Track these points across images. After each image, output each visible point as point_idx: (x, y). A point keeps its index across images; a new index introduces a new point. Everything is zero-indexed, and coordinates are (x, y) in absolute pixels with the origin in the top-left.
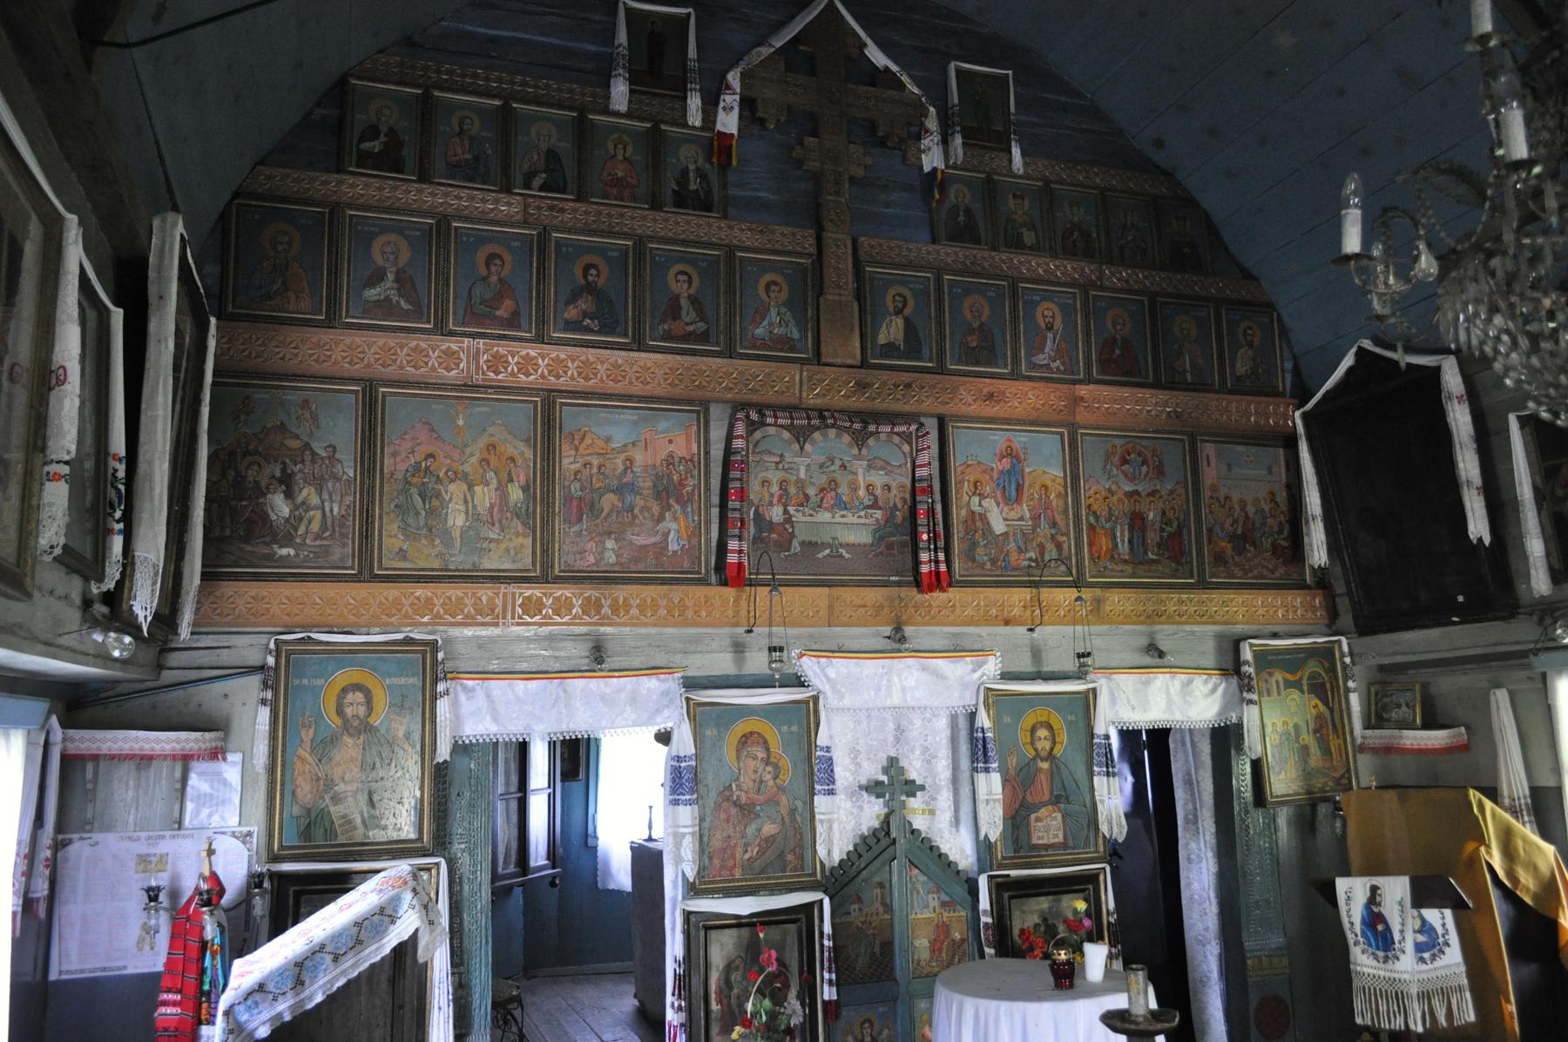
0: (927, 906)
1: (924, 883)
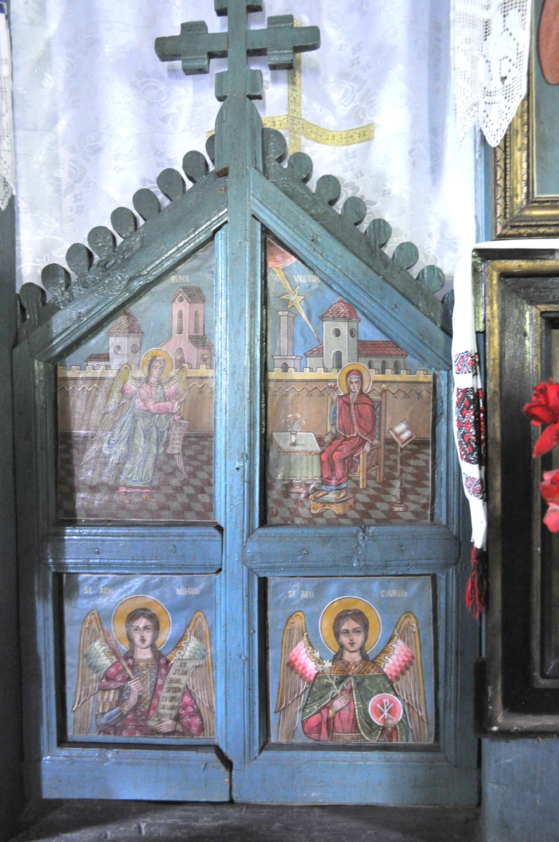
0: (319, 352)
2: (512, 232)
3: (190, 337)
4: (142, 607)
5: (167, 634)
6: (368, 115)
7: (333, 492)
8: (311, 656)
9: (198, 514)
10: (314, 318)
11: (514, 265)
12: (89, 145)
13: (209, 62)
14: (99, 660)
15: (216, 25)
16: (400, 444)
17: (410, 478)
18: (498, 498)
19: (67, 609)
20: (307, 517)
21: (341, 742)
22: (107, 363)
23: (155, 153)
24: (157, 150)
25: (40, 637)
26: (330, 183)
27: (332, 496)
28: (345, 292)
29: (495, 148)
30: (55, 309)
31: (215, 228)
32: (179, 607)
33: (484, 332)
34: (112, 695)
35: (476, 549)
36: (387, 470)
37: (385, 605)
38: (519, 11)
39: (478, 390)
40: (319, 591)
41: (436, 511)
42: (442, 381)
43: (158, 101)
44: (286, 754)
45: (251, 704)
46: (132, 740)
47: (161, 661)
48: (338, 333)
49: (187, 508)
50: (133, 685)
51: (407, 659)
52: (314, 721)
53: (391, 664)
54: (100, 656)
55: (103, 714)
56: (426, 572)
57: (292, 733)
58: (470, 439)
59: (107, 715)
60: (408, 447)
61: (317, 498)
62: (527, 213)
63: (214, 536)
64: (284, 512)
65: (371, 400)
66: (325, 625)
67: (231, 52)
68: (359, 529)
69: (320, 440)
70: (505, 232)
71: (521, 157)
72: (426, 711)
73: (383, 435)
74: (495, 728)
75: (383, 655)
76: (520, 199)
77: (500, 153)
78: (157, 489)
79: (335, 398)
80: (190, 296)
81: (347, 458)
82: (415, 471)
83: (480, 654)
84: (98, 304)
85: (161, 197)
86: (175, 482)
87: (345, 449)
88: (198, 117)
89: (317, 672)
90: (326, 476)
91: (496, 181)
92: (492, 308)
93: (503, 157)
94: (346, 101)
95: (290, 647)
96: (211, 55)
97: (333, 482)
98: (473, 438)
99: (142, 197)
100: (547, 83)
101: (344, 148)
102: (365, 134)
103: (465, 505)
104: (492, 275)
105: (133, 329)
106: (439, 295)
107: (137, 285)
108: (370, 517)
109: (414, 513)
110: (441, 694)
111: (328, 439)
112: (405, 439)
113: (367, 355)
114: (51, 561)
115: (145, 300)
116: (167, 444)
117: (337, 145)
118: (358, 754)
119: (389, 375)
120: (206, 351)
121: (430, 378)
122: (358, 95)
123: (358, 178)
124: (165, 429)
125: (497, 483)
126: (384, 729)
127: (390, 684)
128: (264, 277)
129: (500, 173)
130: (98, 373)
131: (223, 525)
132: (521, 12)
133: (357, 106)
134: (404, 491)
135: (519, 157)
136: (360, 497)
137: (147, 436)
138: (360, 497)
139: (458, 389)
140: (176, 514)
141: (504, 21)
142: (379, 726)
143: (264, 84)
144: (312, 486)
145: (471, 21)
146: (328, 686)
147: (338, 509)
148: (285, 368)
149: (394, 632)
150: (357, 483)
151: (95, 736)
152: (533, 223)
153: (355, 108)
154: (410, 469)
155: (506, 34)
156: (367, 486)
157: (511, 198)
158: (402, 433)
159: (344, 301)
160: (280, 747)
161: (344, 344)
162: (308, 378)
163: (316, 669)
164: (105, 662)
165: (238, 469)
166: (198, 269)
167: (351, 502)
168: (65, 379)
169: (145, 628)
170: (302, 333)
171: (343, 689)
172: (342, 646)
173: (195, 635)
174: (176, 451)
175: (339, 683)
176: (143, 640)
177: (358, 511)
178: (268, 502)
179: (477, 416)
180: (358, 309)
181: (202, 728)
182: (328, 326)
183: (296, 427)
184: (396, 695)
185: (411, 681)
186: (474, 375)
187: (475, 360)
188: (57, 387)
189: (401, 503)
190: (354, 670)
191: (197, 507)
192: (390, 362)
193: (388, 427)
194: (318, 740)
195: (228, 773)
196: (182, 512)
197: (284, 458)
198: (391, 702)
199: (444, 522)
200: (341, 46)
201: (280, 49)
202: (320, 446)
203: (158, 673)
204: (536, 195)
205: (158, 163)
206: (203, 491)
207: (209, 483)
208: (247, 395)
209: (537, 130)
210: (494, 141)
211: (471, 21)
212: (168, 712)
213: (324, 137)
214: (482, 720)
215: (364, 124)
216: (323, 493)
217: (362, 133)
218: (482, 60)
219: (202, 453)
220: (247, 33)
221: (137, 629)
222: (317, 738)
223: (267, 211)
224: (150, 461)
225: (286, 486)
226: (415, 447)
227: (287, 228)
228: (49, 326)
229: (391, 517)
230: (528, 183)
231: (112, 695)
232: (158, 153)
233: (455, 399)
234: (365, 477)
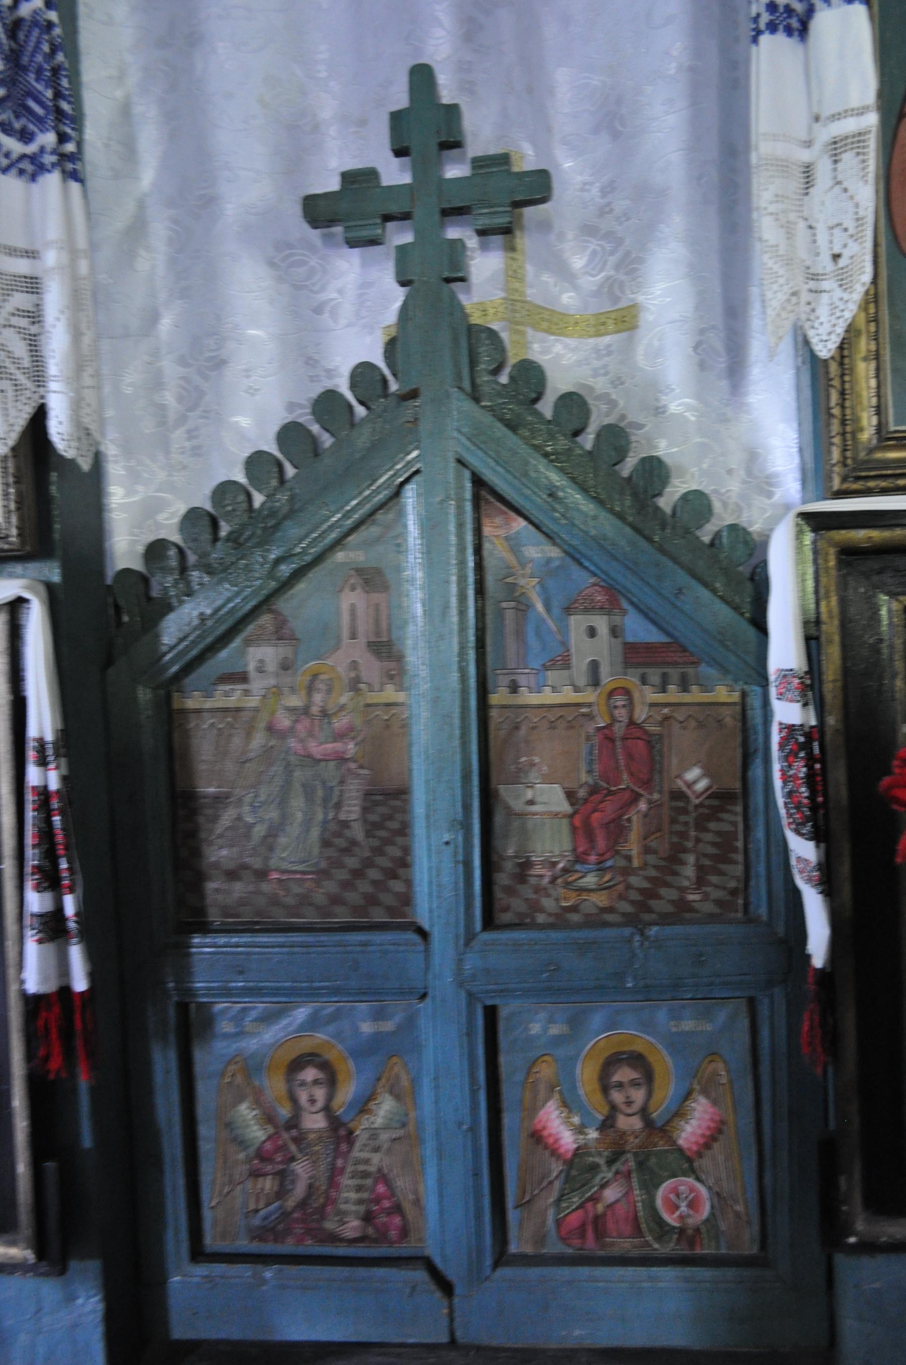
0: (564, 662)
1: (547, 571)
3: (370, 644)
4: (309, 1052)
5: (347, 1092)
6: (628, 292)
7: (594, 874)
8: (567, 1122)
10: (556, 611)
11: (860, 536)
12: (207, 355)
13: (384, 228)
14: (248, 1130)
15: (395, 173)
17: (711, 850)
18: (846, 891)
19: (199, 1056)
20: (555, 912)
21: (616, 1251)
22: (244, 686)
24: (310, 358)
25: (160, 1101)
26: (574, 404)
27: (590, 880)
28: (602, 571)
29: (826, 361)
30: (166, 607)
31: (401, 479)
32: (366, 1050)
33: (817, 638)
34: (268, 1184)
35: (816, 970)
36: (675, 839)
37: (677, 1044)
39: (812, 727)
40: (576, 1022)
41: (752, 899)
42: (755, 702)
43: (307, 283)
44: (534, 1272)
45: (478, 1197)
46: (301, 1250)
47: (340, 1132)
48: (592, 632)
49: (372, 901)
50: (301, 1169)
51: (712, 1125)
52: (575, 1219)
53: (689, 1132)
54: (248, 1126)
55: (256, 1211)
56: (738, 994)
57: (540, 1239)
58: (800, 802)
59: (262, 1213)
60: (707, 802)
62: (879, 455)
63: (414, 945)
64: (518, 905)
65: (646, 732)
66: (586, 1074)
67: (418, 213)
68: (635, 931)
69: (570, 795)
70: (845, 486)
71: (867, 370)
72: (745, 1204)
74: (852, 1240)
75: (676, 1120)
76: (867, 435)
77: (834, 368)
78: (324, 874)
80: (367, 582)
81: (613, 821)
82: (719, 840)
83: (826, 1125)
84: (229, 600)
85: (315, 428)
86: (352, 862)
87: (610, 808)
88: (369, 304)
89: (575, 1146)
90: (581, 849)
91: (829, 409)
92: (829, 602)
93: (839, 373)
95: (534, 1109)
96: (387, 218)
97: (593, 858)
98: (806, 801)
99: (290, 434)
101: (592, 341)
102: (626, 320)
103: (795, 896)
104: (827, 554)
105: (281, 633)
106: (745, 570)
107: (285, 570)
108: (650, 910)
109: (719, 903)
110: (768, 1179)
111: (582, 793)
112: (702, 790)
113: (638, 665)
114: (171, 985)
115: (301, 586)
116: (338, 806)
117: (581, 337)
118: (641, 1272)
119: (673, 694)
120: (393, 665)
121: (736, 697)
122: (612, 260)
125: (845, 869)
126: (682, 1231)
127: (688, 1163)
128: (478, 550)
129: (834, 397)
130: (232, 701)
131: (426, 926)
134: (701, 869)
135: (864, 370)
136: (634, 880)
137: (308, 792)
138: (634, 880)
139: (781, 724)
140: (357, 910)
141: (835, 170)
142: (674, 1228)
143: (469, 253)
144: (561, 865)
145: (782, 166)
146: (594, 1168)
147: (600, 900)
148: (514, 688)
149: (692, 1084)
150: (629, 858)
151: (244, 1245)
153: (608, 278)
154: (709, 837)
155: (837, 189)
157: (853, 434)
158: (695, 782)
159: (602, 584)
160: (525, 1260)
161: (603, 649)
162: (548, 702)
163: (575, 1142)
164: (257, 1133)
165: (447, 843)
166: (378, 540)
167: (621, 887)
168: (184, 712)
169: (316, 1082)
170: (538, 633)
171: (617, 1173)
172: (614, 1108)
173: (391, 1092)
174: (353, 816)
175: (610, 1162)
176: (312, 1101)
177: (632, 902)
178: (496, 888)
179: (810, 767)
180: (624, 596)
181: (404, 1232)
182: (577, 623)
183: (533, 776)
184: (698, 1179)
185: (720, 1158)
188: (172, 722)
190: (633, 1142)
191: (387, 899)
192: (674, 673)
193: (674, 772)
194: (581, 1249)
195: (445, 1302)
197: (516, 824)
198: (692, 1190)
199: (765, 918)
200: (585, 184)
202: (572, 804)
203: (336, 1149)
206: (395, 877)
207: (404, 862)
208: (457, 732)
209: (891, 326)
210: (825, 349)
212: (354, 1208)
214: (832, 1230)
215: (622, 304)
216: (576, 876)
218: (802, 225)
219: (390, 818)
220: (442, 181)
221: (303, 1084)
222: (580, 1246)
223: (479, 453)
224: (315, 833)
225: (521, 865)
226: (716, 802)
227: (509, 477)
228: (157, 636)
229: (681, 911)
230: (879, 410)
231: (268, 1184)
233: (775, 738)
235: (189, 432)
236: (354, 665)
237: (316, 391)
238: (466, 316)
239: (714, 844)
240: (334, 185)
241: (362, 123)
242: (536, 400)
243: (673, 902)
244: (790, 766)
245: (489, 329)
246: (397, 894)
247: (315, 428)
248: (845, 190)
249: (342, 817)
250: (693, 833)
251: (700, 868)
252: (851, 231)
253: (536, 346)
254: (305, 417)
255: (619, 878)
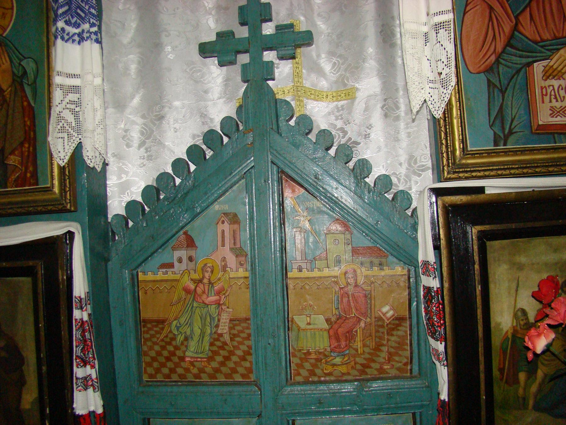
2: (453, 176)
9: (243, 376)
13: (236, 57)
16: (386, 321)
22: (172, 270)
23: (201, 116)
24: (202, 114)
27: (338, 360)
38: (446, 30)
39: (437, 288)
61: (328, 362)
67: (251, 50)
69: (327, 320)
73: (373, 316)
77: (442, 121)
79: (337, 289)
85: (204, 147)
94: (334, 71)
96: (239, 52)
99: (194, 152)
100: (470, 72)
101: (336, 103)
109: (398, 369)
111: (333, 319)
116: (217, 326)
121: (405, 272)
122: (343, 67)
123: (346, 125)
124: (215, 315)
132: (447, 31)
133: (342, 75)
136: (358, 359)
139: (424, 286)
145: (414, 36)
148: (300, 270)
150: (357, 350)
152: (468, 169)
153: (341, 75)
154: (393, 338)
156: (364, 351)
158: (387, 312)
167: (353, 363)
174: (225, 331)
186: (433, 278)
187: (434, 267)
189: (389, 363)
196: (231, 375)
200: (329, 33)
201: (285, 47)
204: (469, 149)
205: (203, 122)
206: (245, 360)
211: (414, 36)
213: (320, 96)
216: (332, 358)
217: (347, 94)
224: (207, 339)
226: (397, 322)
232: (203, 115)
234: (362, 345)
235: (146, 149)
236: (224, 259)
237: (206, 129)
238: (274, 94)
239: (396, 342)
240: (213, 38)
241: (227, 9)
242: (307, 134)
243: (376, 369)
244: (428, 307)
245: (285, 100)
246: (246, 368)
247: (204, 147)
248: (442, 45)
249: (219, 331)
250: (386, 337)
251: (390, 353)
252: (445, 63)
253: (309, 107)
254: (199, 142)
255: (352, 359)
